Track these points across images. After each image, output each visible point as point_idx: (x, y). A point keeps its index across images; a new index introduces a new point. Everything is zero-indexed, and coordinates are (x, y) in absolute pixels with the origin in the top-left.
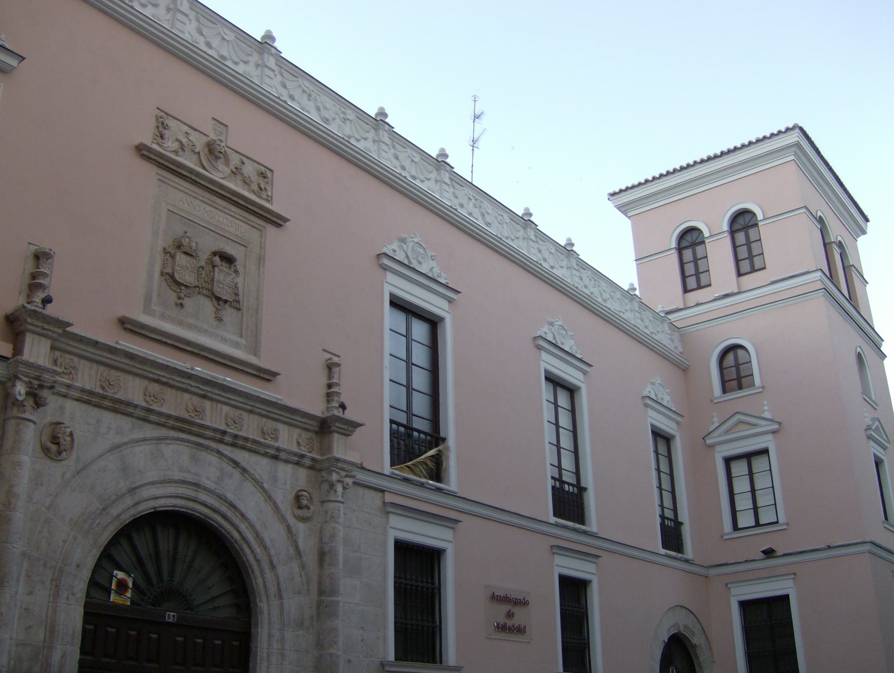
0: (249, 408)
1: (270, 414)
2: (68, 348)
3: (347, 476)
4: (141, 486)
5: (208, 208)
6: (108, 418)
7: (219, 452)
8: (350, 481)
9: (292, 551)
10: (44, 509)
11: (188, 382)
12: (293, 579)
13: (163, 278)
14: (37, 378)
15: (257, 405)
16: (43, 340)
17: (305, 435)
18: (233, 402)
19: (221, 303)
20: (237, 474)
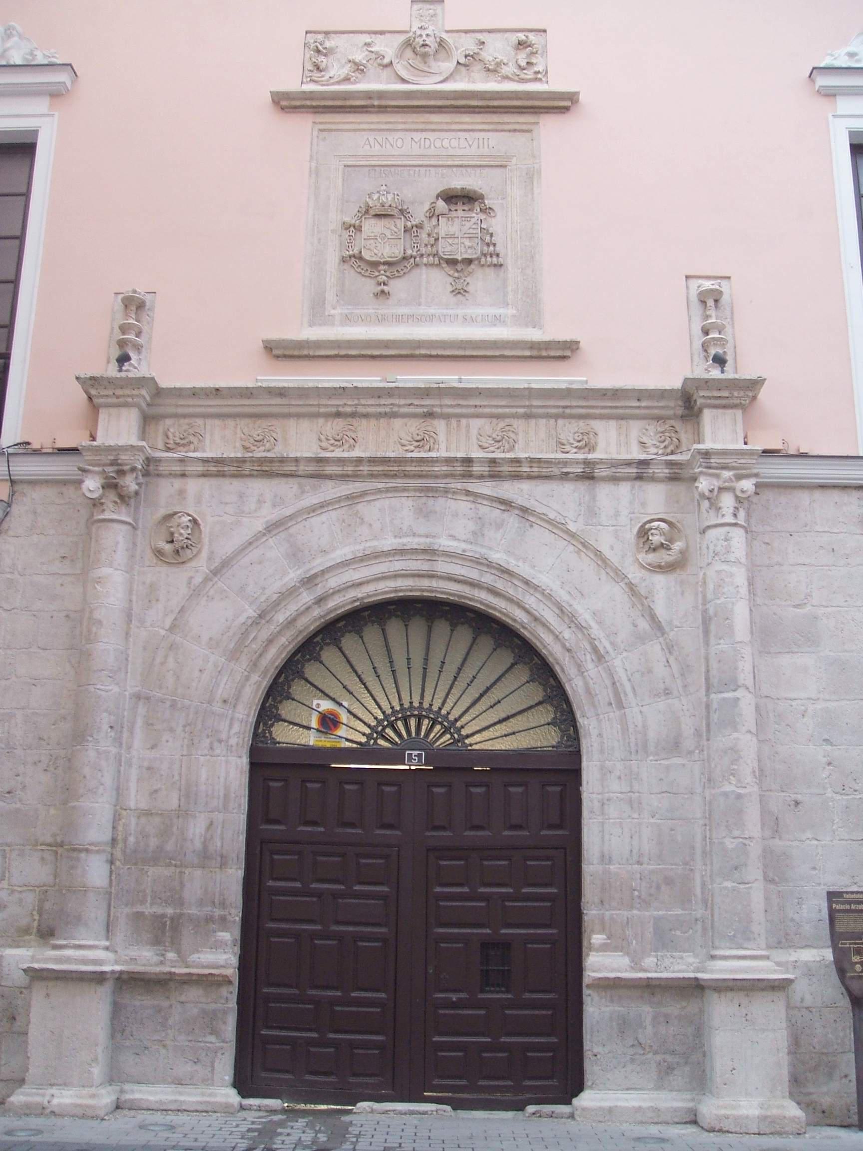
0: (521, 410)
1: (568, 411)
2: (180, 411)
3: (739, 478)
4: (323, 572)
5: (417, 136)
6: (258, 487)
7: (468, 493)
8: (747, 485)
9: (644, 625)
10: (163, 632)
11: (390, 401)
12: (650, 671)
13: (346, 266)
14: (114, 463)
15: (535, 403)
16: (124, 411)
17: (653, 428)
18: (487, 410)
19: (459, 267)
20: (512, 520)
